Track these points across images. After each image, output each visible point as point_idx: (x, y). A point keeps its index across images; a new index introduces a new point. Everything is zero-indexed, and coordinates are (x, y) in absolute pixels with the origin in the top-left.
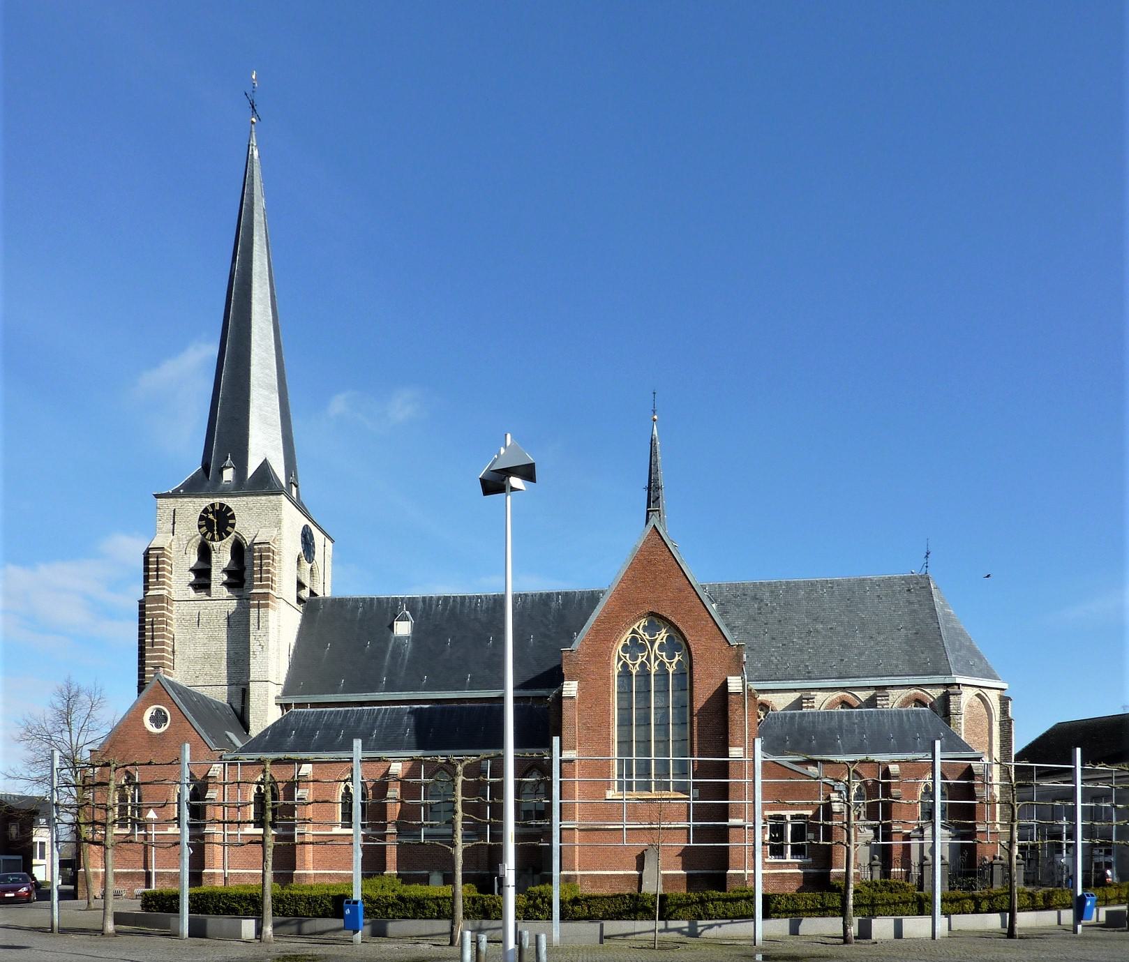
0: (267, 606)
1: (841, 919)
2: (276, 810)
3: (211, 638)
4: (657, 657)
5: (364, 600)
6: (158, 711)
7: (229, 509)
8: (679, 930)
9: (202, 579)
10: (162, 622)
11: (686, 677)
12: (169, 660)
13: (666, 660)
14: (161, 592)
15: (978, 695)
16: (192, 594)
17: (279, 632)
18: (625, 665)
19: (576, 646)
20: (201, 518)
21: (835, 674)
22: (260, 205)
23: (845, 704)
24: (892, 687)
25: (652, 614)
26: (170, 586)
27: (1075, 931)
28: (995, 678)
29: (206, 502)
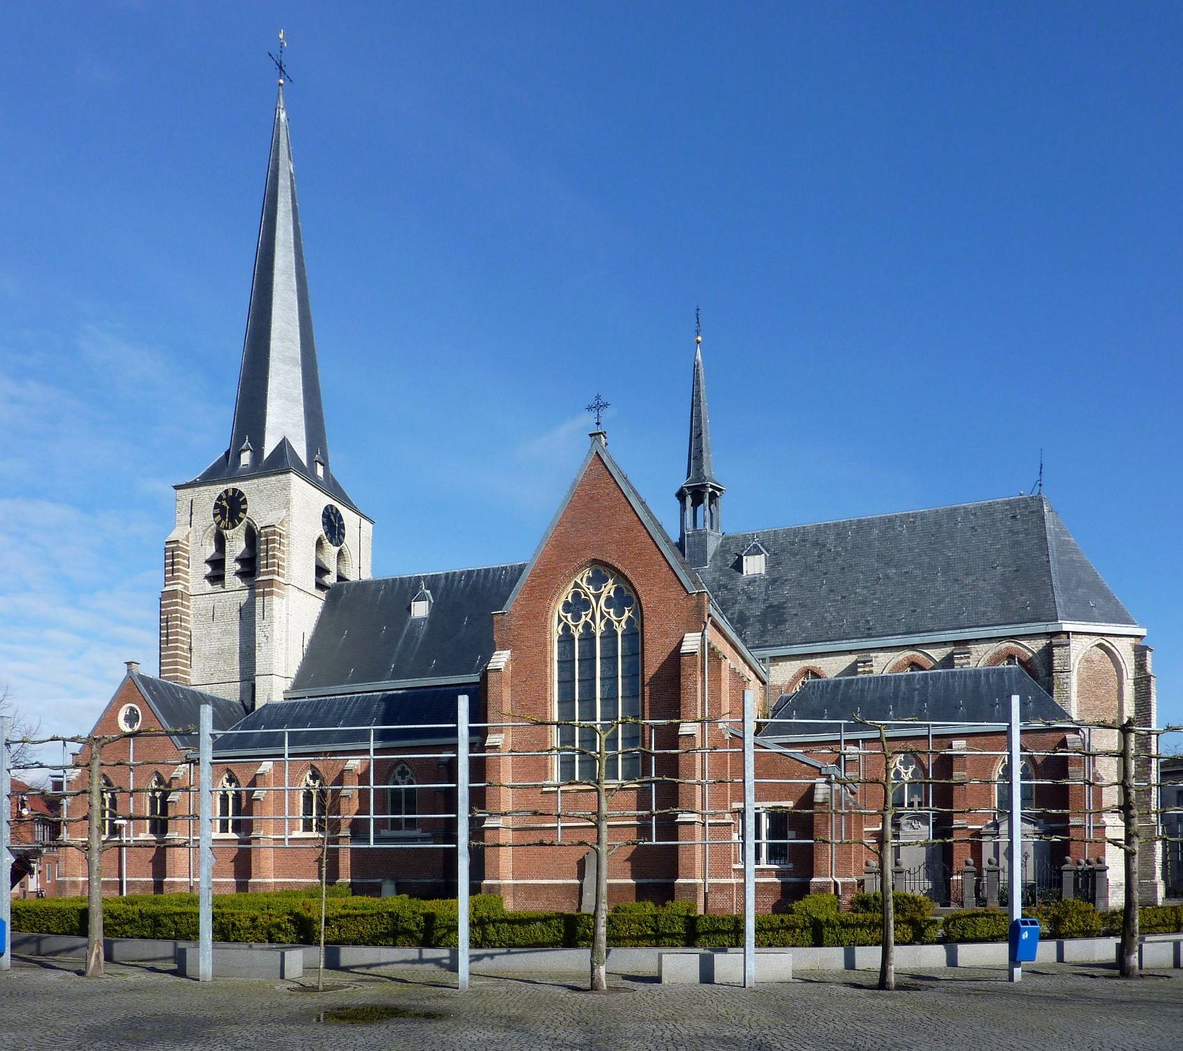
0: (271, 593)
1: (589, 951)
3: (225, 632)
4: (602, 615)
5: (386, 581)
6: (132, 709)
7: (241, 494)
8: (437, 961)
10: (176, 619)
11: (635, 636)
12: (186, 658)
13: (614, 618)
14: (175, 587)
15: (1100, 646)
16: (208, 587)
17: (292, 618)
18: (566, 628)
19: (509, 607)
20: (216, 506)
21: (903, 629)
22: (286, 167)
23: (914, 665)
24: (977, 641)
25: (595, 562)
26: (187, 581)
27: (1011, 978)
28: (1127, 621)
29: (219, 489)
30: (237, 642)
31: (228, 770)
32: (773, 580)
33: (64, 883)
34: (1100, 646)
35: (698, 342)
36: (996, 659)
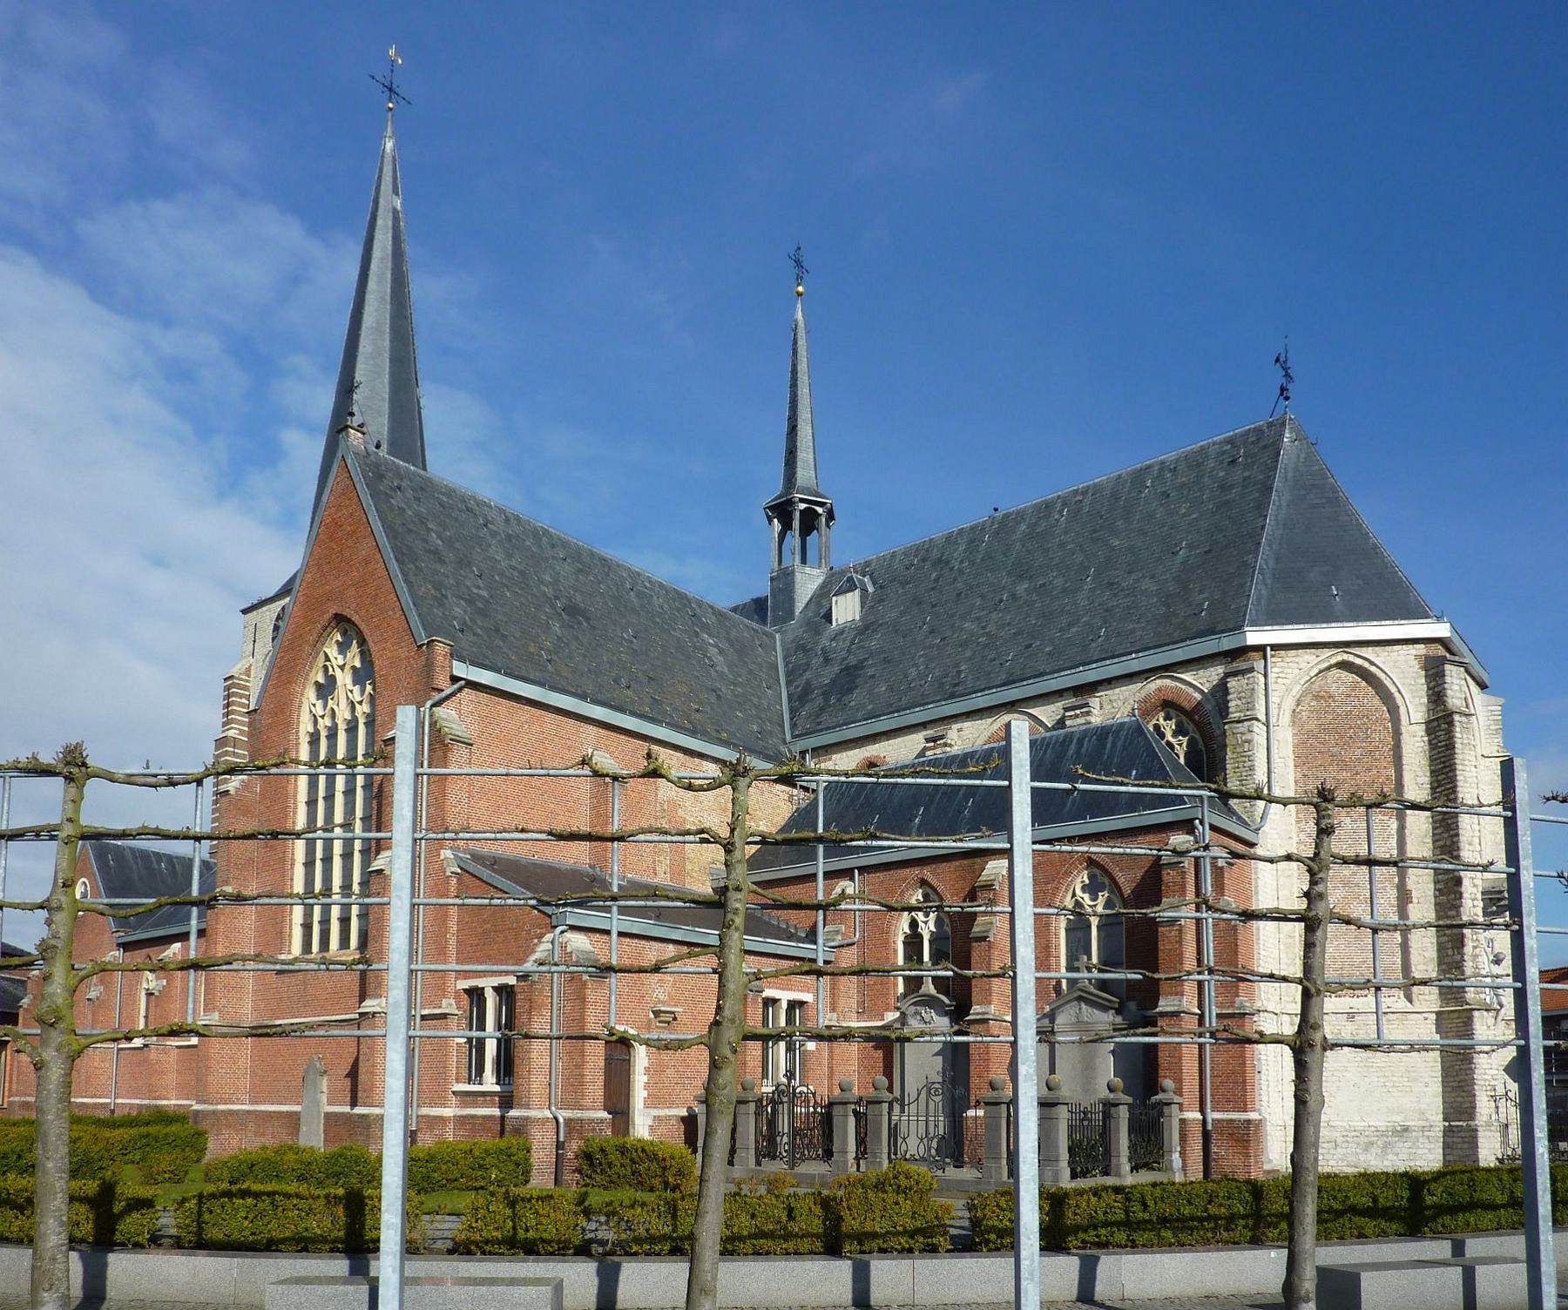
15: (1344, 666)
24: (1110, 682)
32: (865, 628)
34: (1344, 666)
35: (800, 294)
36: (1147, 710)
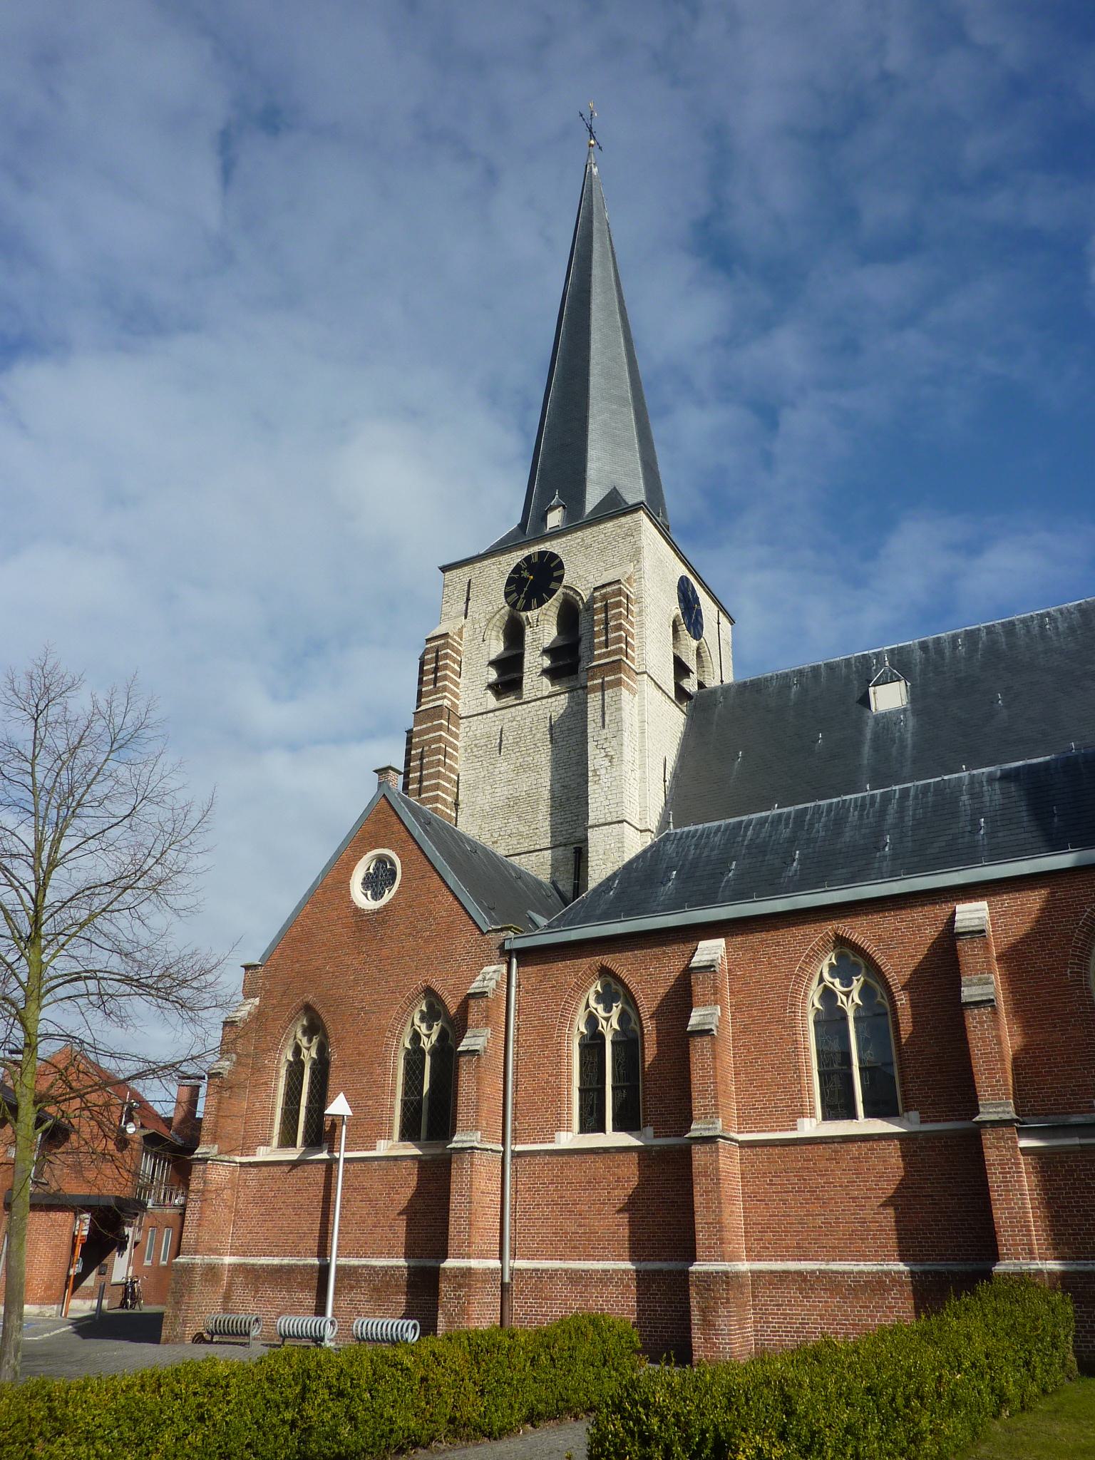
0: (619, 683)
2: (649, 1082)
3: (520, 769)
6: (381, 860)
9: (508, 677)
10: (438, 751)
16: (491, 701)
26: (456, 696)
29: (517, 557)
30: (545, 778)
31: (605, 972)
33: (188, 1269)
